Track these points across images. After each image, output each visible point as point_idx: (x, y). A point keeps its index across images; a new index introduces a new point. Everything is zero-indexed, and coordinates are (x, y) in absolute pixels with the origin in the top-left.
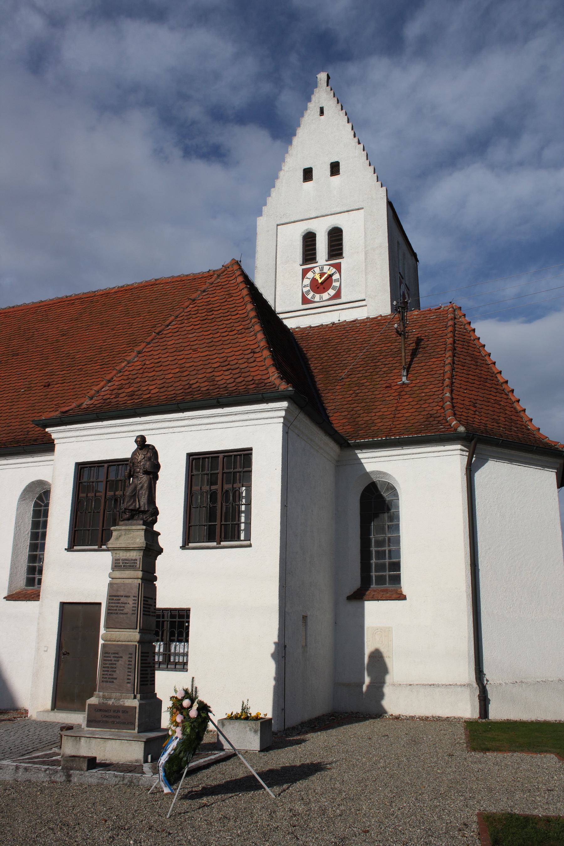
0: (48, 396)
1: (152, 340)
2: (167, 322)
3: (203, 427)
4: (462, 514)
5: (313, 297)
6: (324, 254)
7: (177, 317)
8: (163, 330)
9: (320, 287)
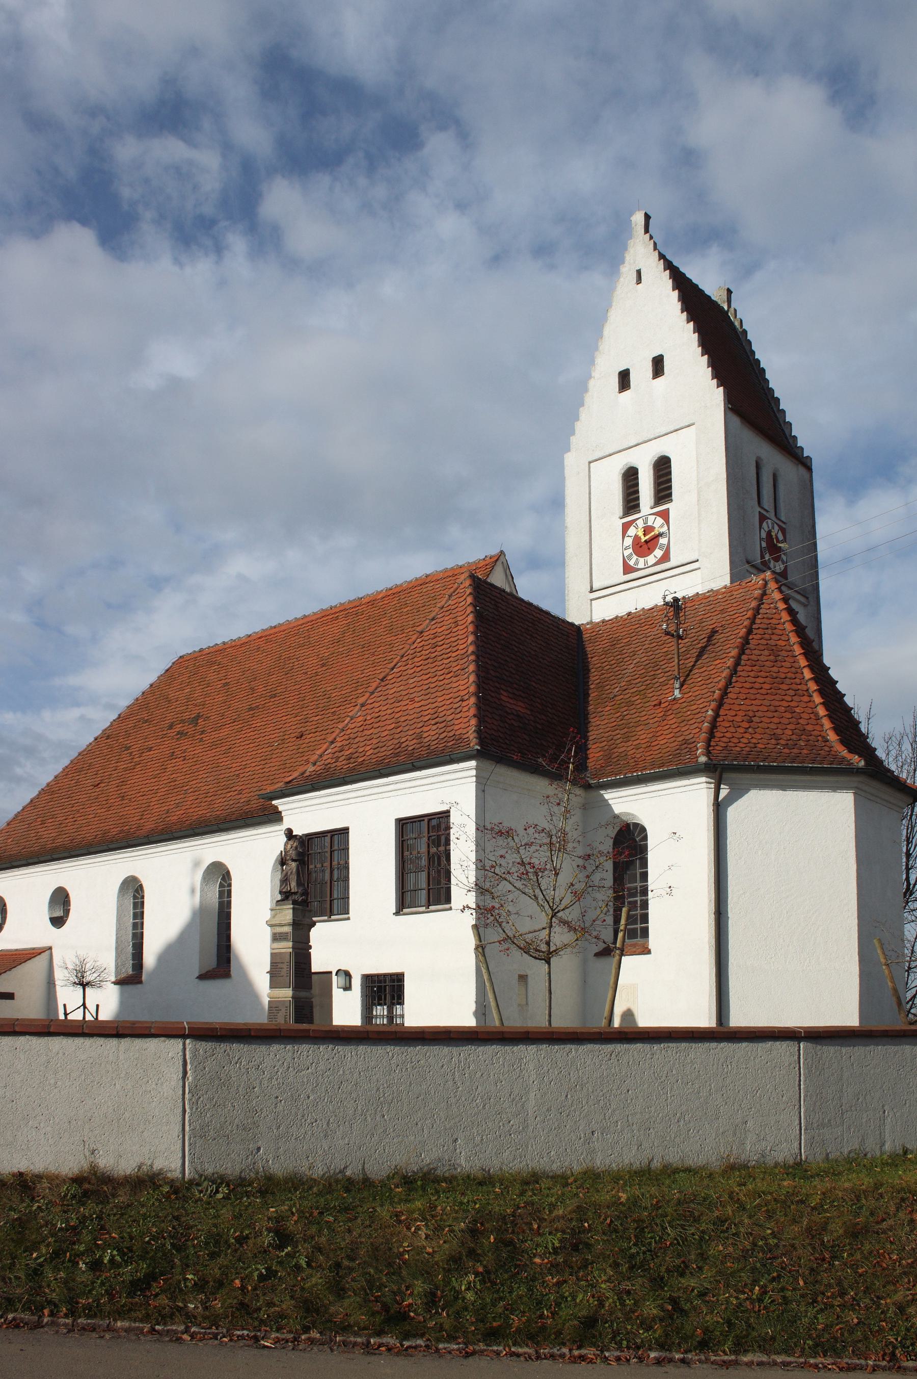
0: (300, 750)
1: (376, 689)
2: (392, 665)
3: (407, 791)
4: (706, 857)
5: (637, 563)
6: (648, 499)
7: (402, 656)
8: (388, 675)
9: (644, 547)
